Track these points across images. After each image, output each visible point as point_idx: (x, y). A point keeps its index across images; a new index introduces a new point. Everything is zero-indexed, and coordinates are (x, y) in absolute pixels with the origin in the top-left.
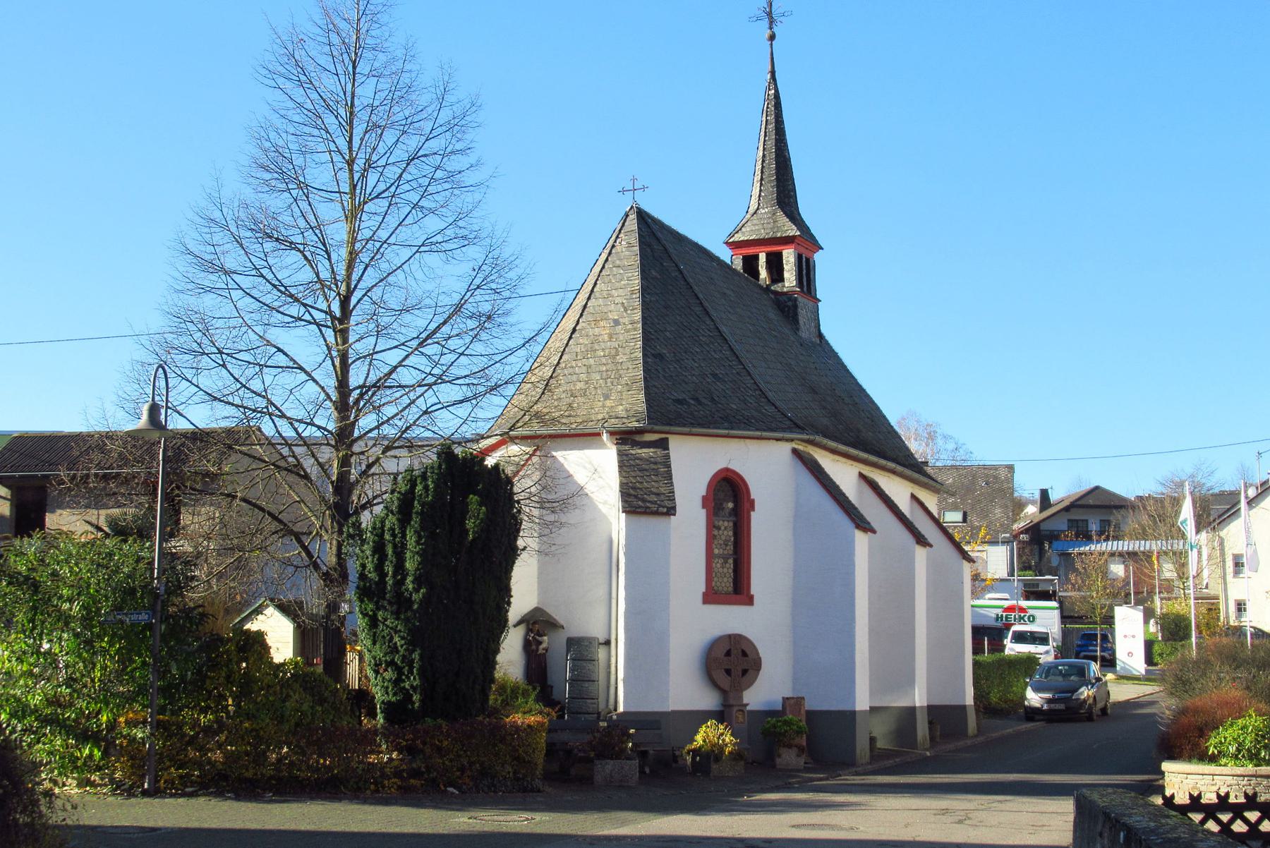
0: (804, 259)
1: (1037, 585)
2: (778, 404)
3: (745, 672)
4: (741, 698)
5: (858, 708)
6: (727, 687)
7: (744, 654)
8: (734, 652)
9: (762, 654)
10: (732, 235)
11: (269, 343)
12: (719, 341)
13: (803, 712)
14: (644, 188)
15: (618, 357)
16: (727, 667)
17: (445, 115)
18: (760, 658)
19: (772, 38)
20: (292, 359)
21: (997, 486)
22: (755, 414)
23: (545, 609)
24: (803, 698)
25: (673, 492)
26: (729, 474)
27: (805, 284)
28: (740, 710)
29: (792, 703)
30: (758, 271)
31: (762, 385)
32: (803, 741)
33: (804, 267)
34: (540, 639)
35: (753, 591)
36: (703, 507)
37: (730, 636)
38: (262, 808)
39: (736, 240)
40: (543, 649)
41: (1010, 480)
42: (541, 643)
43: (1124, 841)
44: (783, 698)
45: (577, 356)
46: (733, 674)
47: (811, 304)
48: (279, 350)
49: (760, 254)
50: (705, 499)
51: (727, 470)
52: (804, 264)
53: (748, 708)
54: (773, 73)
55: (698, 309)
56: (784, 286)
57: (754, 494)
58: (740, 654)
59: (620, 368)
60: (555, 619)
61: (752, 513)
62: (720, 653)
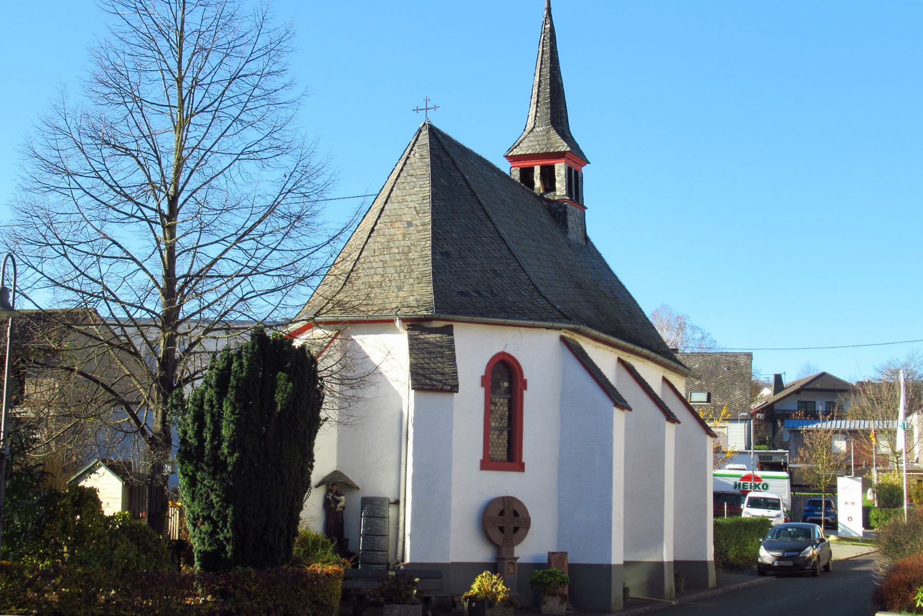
0: (573, 172)
1: (771, 457)
2: (548, 297)
4: (512, 552)
5: (613, 563)
6: (500, 543)
7: (516, 514)
8: (507, 512)
9: (531, 514)
10: (511, 150)
11: (105, 237)
12: (498, 242)
13: (566, 565)
14: (435, 108)
15: (410, 254)
16: (501, 525)
17: (262, 41)
18: (529, 518)
20: (125, 251)
21: (737, 371)
22: (529, 305)
23: (342, 472)
24: (567, 553)
25: (457, 372)
26: (505, 357)
27: (574, 193)
28: (511, 563)
29: (557, 557)
30: (534, 181)
31: (535, 281)
32: (566, 591)
33: (573, 178)
34: (338, 498)
36: (482, 386)
37: (503, 498)
39: (515, 154)
40: (341, 507)
41: (749, 366)
42: (338, 502)
45: (374, 253)
46: (505, 531)
47: (578, 211)
48: (115, 242)
49: (535, 167)
50: (484, 379)
51: (503, 354)
52: (573, 176)
53: (519, 561)
54: (549, 9)
55: (480, 214)
56: (555, 195)
58: (512, 514)
59: (411, 263)
60: (352, 482)
61: (524, 391)
62: (495, 513)
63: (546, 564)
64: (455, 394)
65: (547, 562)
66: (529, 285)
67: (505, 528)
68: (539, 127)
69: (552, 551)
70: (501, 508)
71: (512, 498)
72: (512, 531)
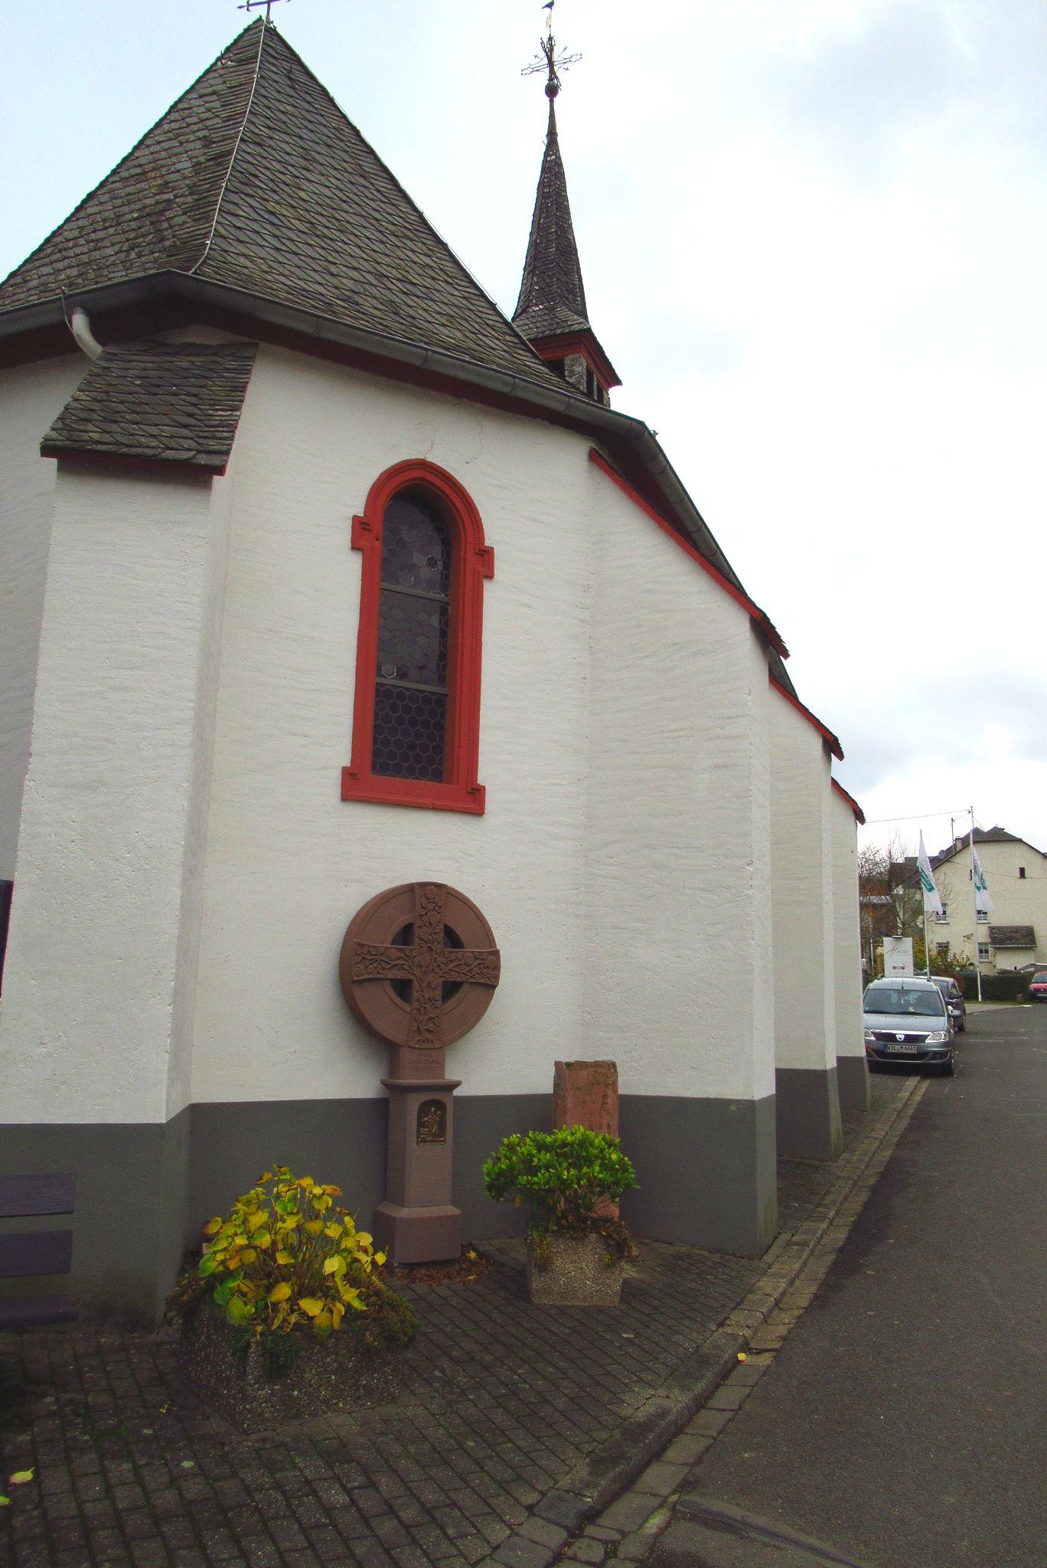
3: (451, 989)
4: (439, 1066)
7: (453, 939)
13: (611, 1101)
16: (399, 974)
18: (496, 953)
19: (552, 91)
24: (613, 1065)
26: (431, 478)
35: (485, 775)
36: (355, 547)
37: (411, 889)
38: (481, 505)
43: (982, 999)
44: (557, 1064)
50: (361, 528)
51: (423, 465)
54: (552, 134)
57: (493, 536)
58: (441, 937)
62: (383, 938)
63: (9, 1481)
64: (216, 479)
65: (56, 459)
66: (505, 333)
67: (416, 985)
68: (537, 305)
69: (566, 1058)
70: (404, 920)
71: (440, 887)
72: (439, 993)
